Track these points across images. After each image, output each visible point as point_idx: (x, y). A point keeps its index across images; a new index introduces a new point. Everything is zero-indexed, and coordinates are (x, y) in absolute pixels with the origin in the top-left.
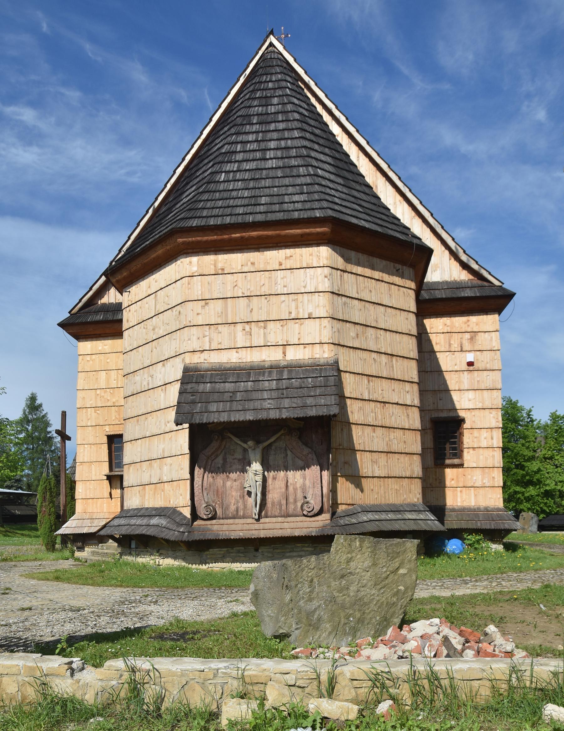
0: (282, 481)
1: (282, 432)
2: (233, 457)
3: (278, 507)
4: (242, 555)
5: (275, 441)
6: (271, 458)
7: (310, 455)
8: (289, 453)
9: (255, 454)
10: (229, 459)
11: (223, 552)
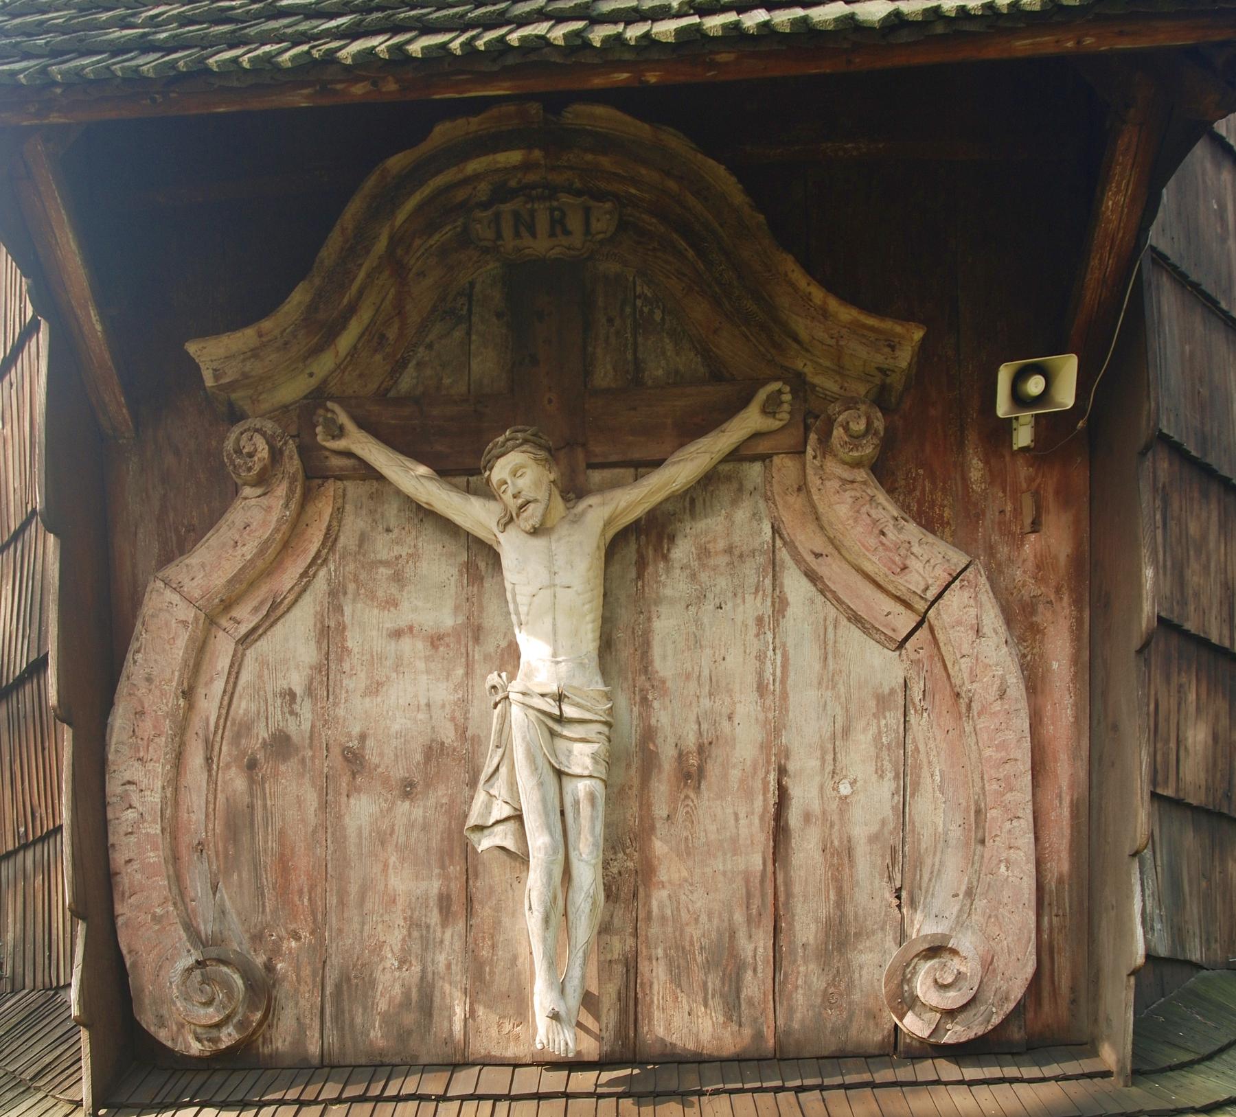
0: (749, 795)
1: (750, 421)
2: (391, 620)
5: (694, 499)
6: (666, 626)
7: (956, 599)
8: (796, 586)
10: (366, 627)
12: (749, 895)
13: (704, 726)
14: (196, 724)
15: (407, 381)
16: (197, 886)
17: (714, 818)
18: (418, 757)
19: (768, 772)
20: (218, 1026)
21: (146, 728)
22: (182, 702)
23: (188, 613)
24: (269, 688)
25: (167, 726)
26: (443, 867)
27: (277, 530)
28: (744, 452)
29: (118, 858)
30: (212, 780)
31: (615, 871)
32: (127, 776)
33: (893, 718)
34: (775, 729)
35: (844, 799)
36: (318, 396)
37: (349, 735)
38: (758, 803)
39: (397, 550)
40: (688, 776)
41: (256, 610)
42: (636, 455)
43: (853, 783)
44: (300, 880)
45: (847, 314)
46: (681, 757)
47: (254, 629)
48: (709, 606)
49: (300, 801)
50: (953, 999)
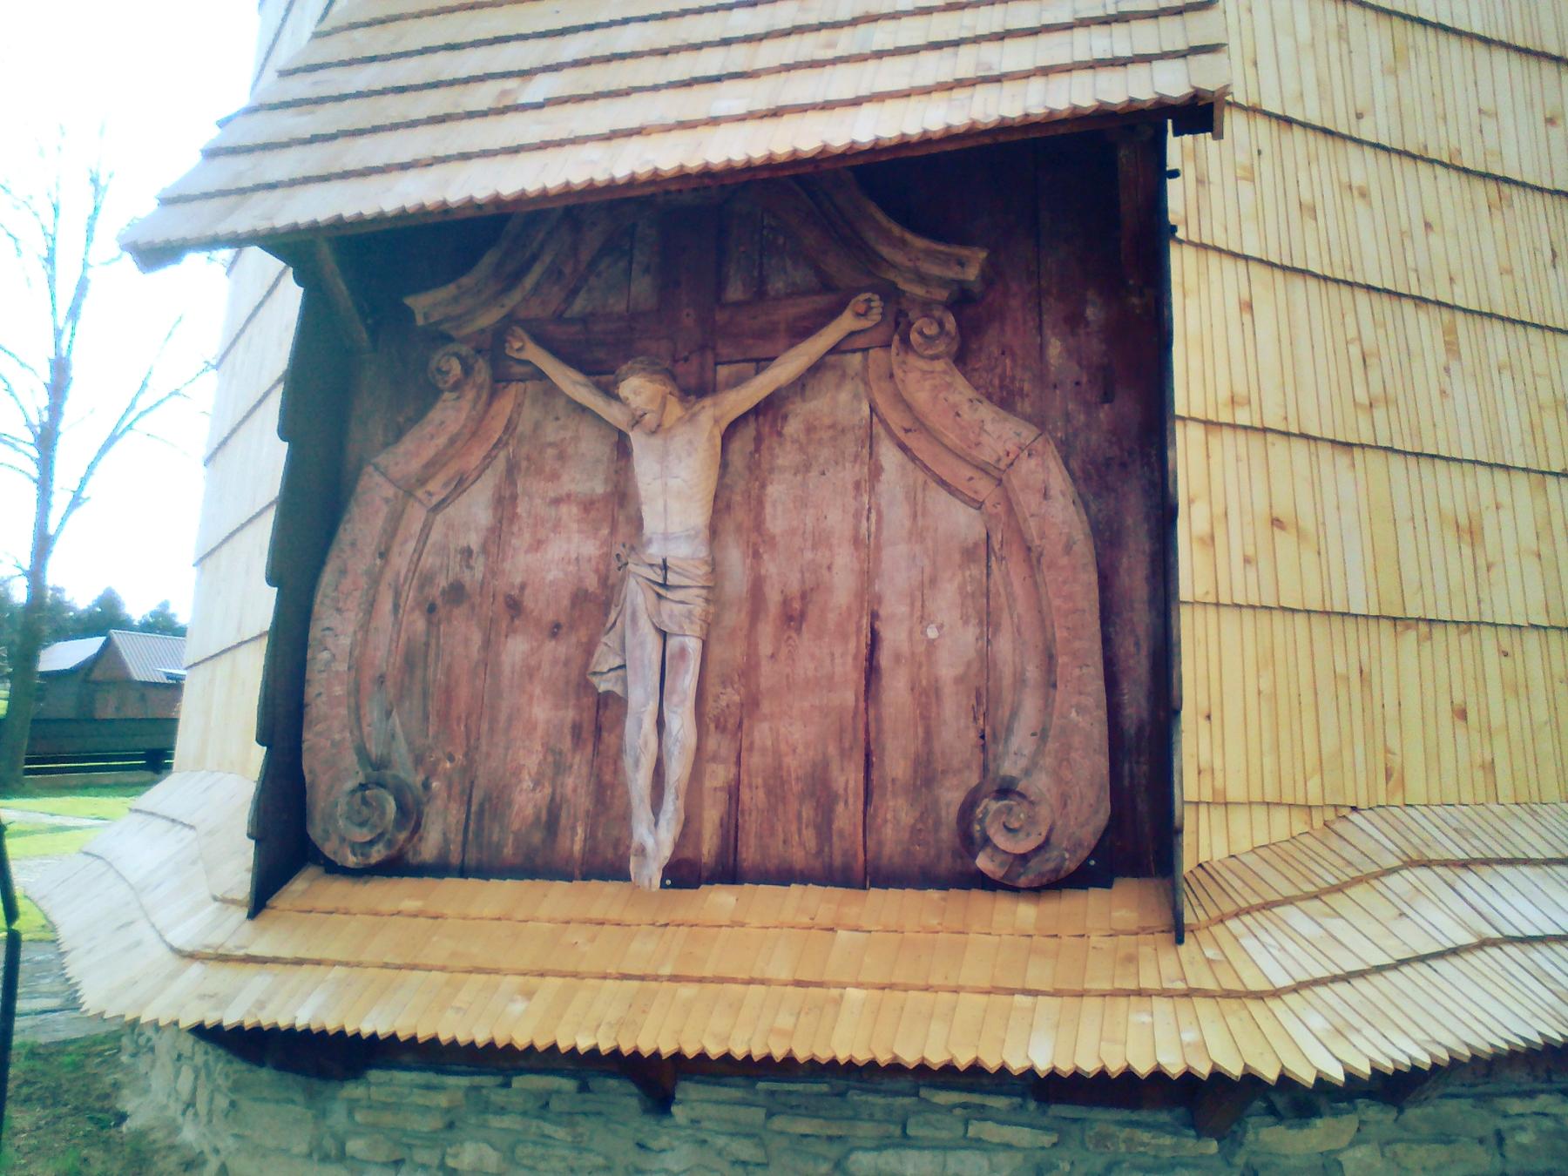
0: (845, 637)
3: (807, 812)
4: (560, 1133)
5: (801, 384)
8: (889, 456)
9: (664, 457)
10: (533, 497)
11: (442, 1100)
12: (842, 731)
13: (807, 575)
14: (389, 576)
15: (579, 305)
16: (372, 713)
17: (813, 657)
18: (566, 602)
19: (861, 617)
20: (371, 843)
21: (347, 584)
22: (378, 562)
23: (389, 491)
24: (452, 547)
25: (363, 582)
26: (578, 699)
27: (464, 426)
28: (844, 348)
29: (311, 692)
30: (397, 622)
31: (724, 704)
32: (326, 624)
33: (976, 571)
34: (868, 576)
35: (931, 644)
36: (510, 320)
37: (513, 586)
38: (852, 645)
39: (562, 434)
40: (790, 618)
41: (446, 485)
42: (755, 355)
43: (940, 627)
44: (460, 707)
45: (920, 243)
46: (786, 602)
47: (444, 500)
48: (814, 473)
49: (467, 641)
50: (1023, 845)
